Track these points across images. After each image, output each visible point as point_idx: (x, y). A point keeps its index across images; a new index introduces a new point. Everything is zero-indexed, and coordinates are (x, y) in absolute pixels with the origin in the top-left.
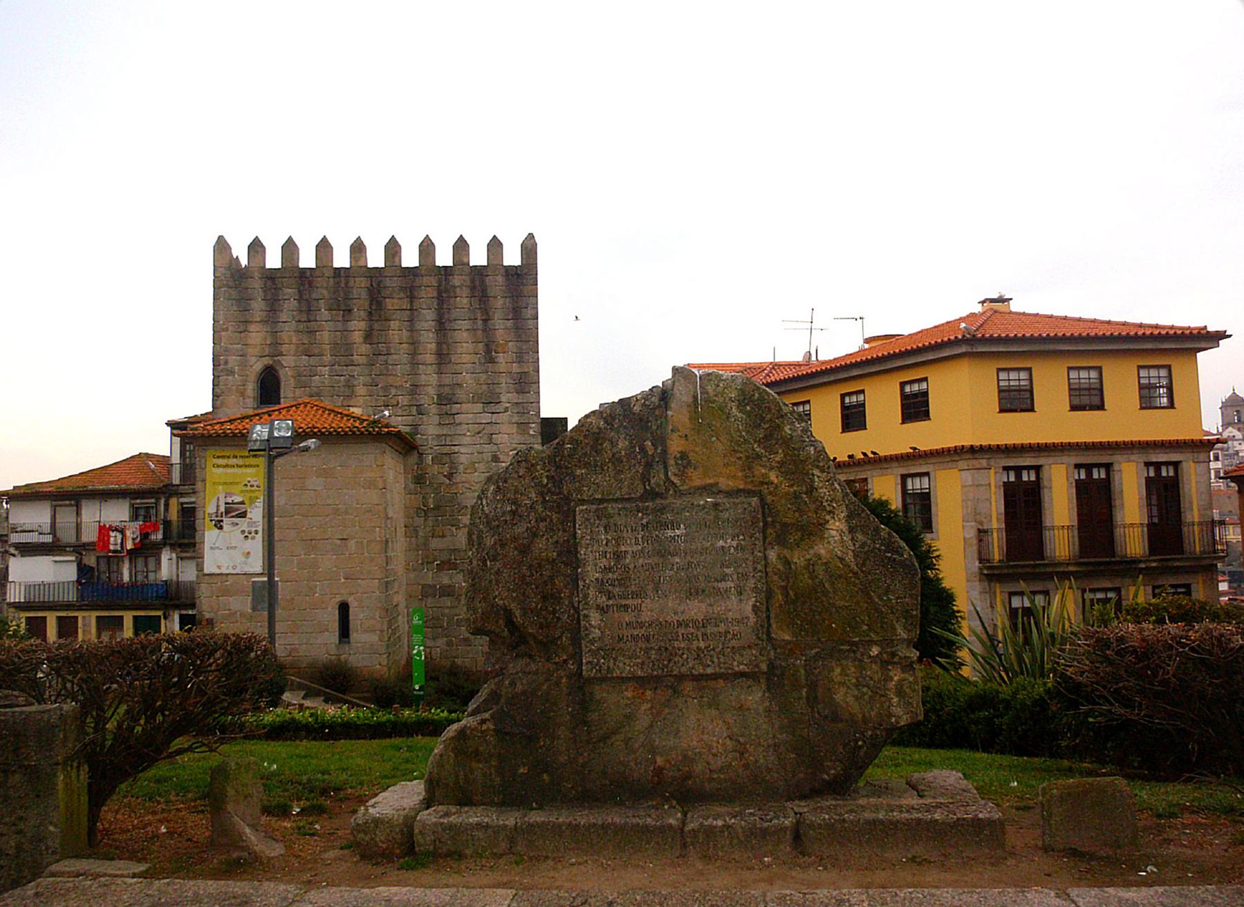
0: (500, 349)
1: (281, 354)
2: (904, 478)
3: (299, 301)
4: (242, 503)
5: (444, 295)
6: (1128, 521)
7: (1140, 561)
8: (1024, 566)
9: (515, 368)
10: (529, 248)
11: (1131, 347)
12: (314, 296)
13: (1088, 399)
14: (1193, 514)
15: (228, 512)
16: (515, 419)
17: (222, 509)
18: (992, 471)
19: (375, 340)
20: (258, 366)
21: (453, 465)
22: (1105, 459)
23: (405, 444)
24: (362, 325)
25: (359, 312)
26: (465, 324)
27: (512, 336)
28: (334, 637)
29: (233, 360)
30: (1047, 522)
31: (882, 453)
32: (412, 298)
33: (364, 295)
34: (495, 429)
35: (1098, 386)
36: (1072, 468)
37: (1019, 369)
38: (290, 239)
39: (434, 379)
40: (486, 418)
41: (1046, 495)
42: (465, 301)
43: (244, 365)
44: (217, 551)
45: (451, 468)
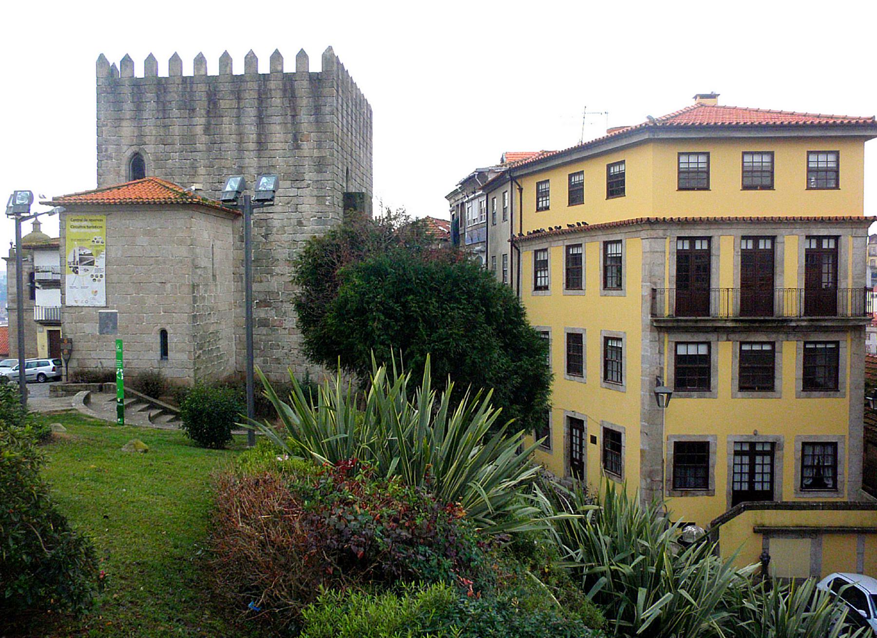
0: (303, 139)
1: (145, 144)
2: (606, 244)
3: (157, 102)
4: (91, 254)
5: (263, 97)
6: (787, 286)
7: (791, 321)
8: (686, 321)
9: (316, 153)
10: (329, 58)
11: (801, 134)
12: (168, 98)
13: (758, 180)
14: (847, 282)
15: (81, 261)
16: (315, 193)
17: (77, 259)
18: (668, 240)
19: (212, 132)
20: (128, 153)
21: (269, 228)
22: (769, 232)
23: (231, 210)
24: (203, 121)
25: (200, 111)
26: (278, 119)
27: (314, 128)
28: (157, 354)
29: (111, 148)
30: (713, 285)
31: (591, 223)
32: (239, 99)
33: (204, 94)
34: (301, 200)
35: (769, 169)
36: (738, 240)
37: (698, 154)
38: (151, 56)
39: (254, 162)
40: (293, 192)
41: (714, 259)
42: (279, 101)
43: (118, 151)
44: (75, 290)
45: (266, 230)
